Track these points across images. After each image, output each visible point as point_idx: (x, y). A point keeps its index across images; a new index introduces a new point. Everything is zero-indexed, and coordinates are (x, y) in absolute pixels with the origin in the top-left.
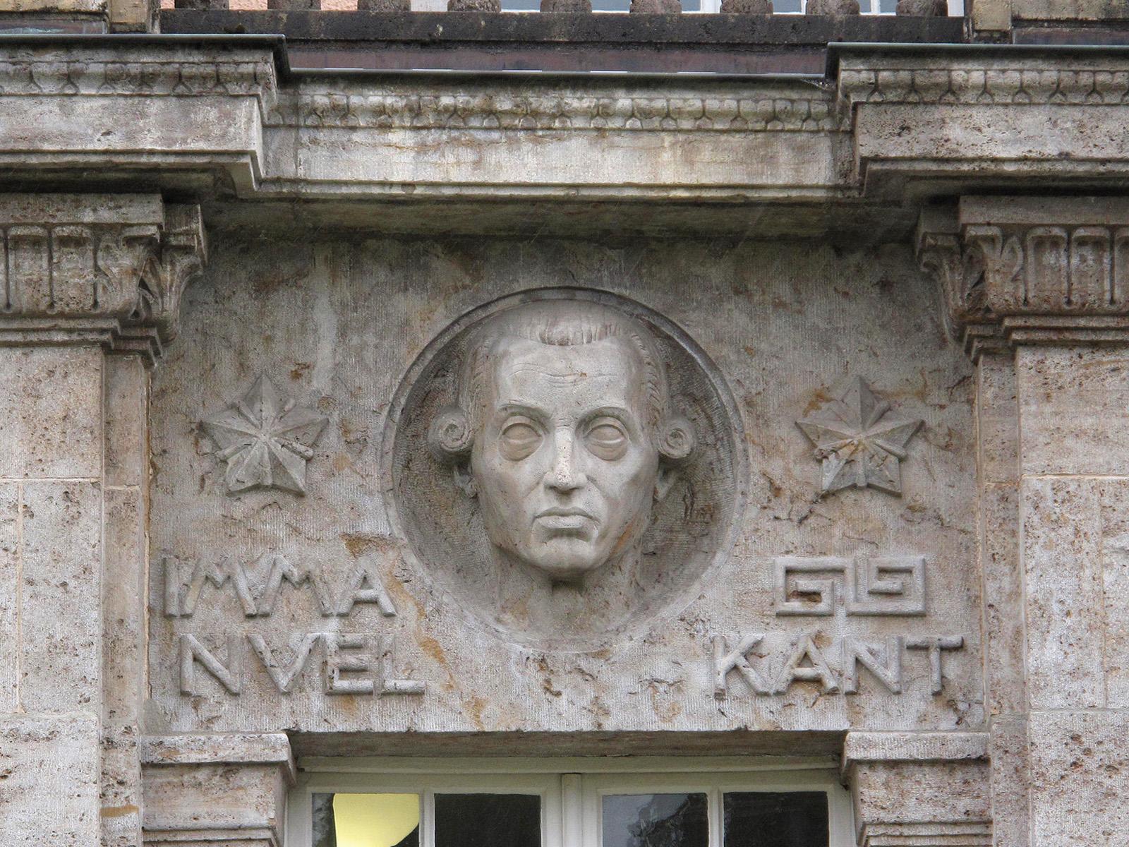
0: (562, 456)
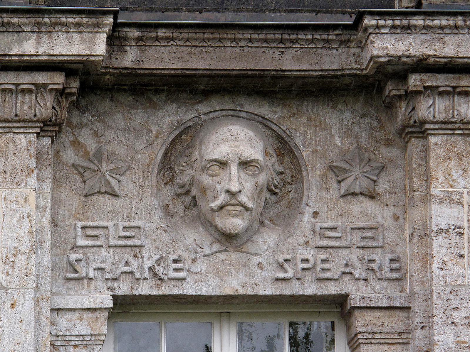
0: (235, 180)
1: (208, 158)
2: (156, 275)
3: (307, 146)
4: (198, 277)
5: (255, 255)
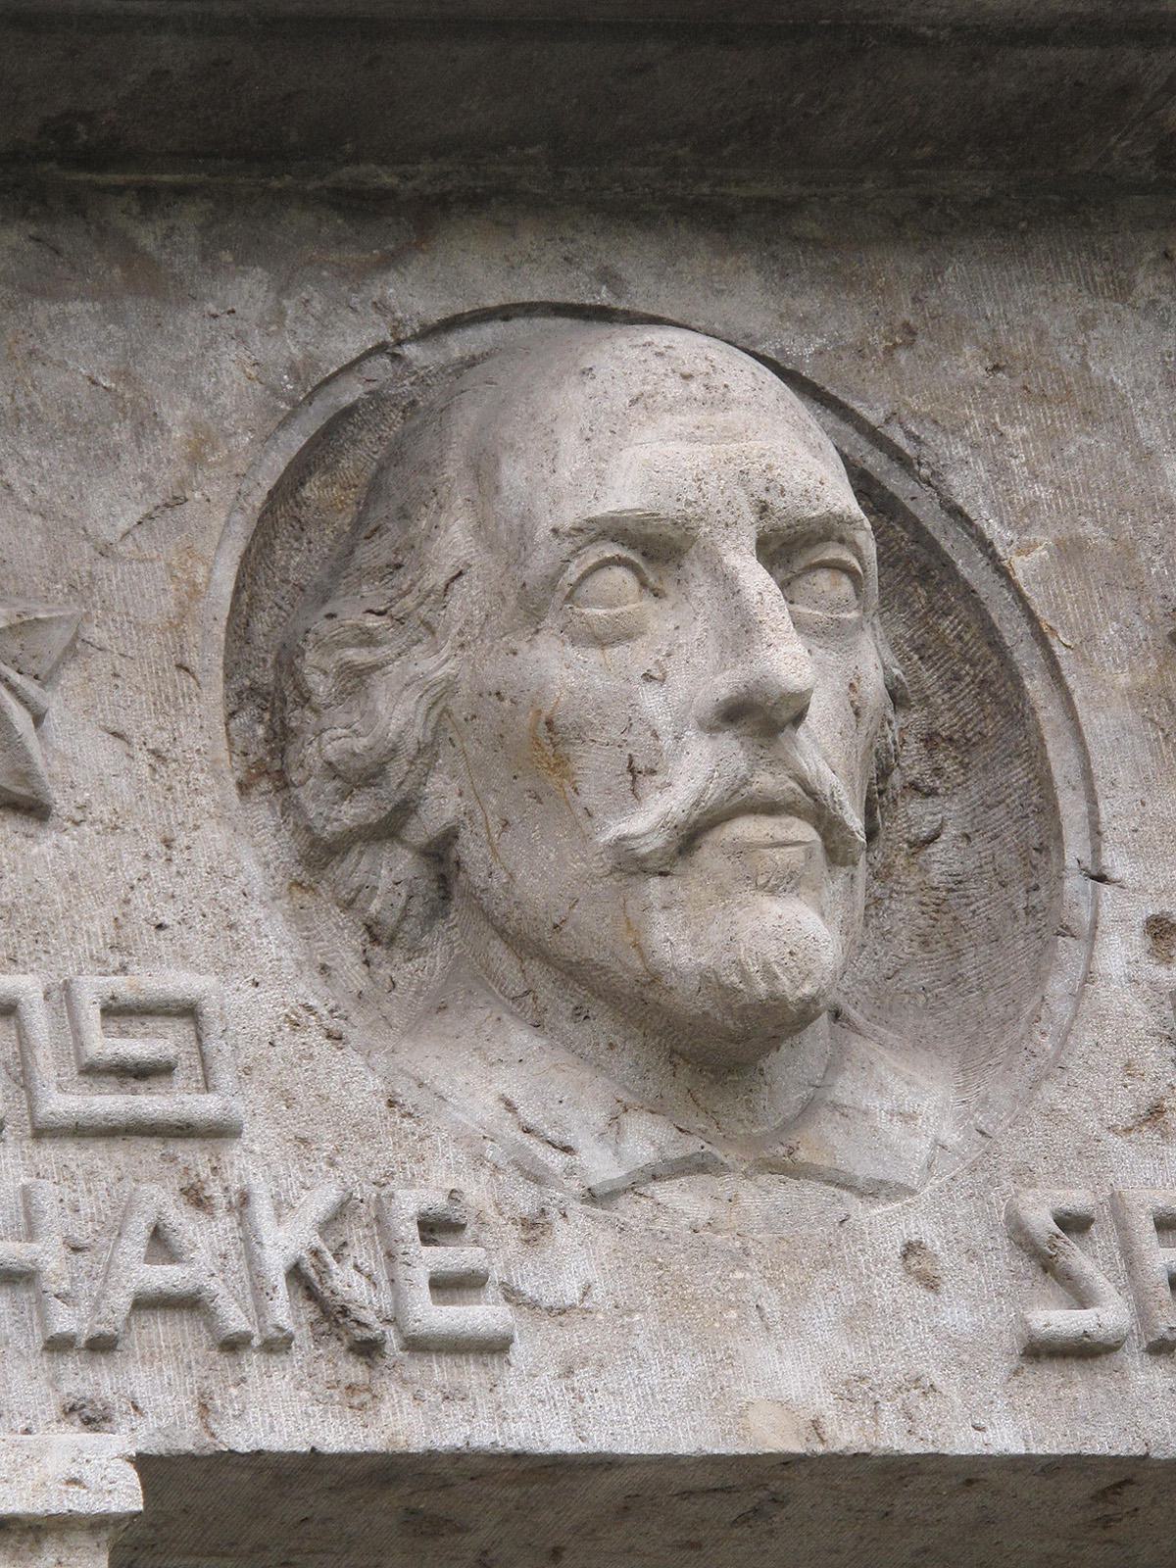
1: (570, 515)
2: (332, 1316)
3: (1024, 516)
4: (575, 1337)
5: (875, 1190)
